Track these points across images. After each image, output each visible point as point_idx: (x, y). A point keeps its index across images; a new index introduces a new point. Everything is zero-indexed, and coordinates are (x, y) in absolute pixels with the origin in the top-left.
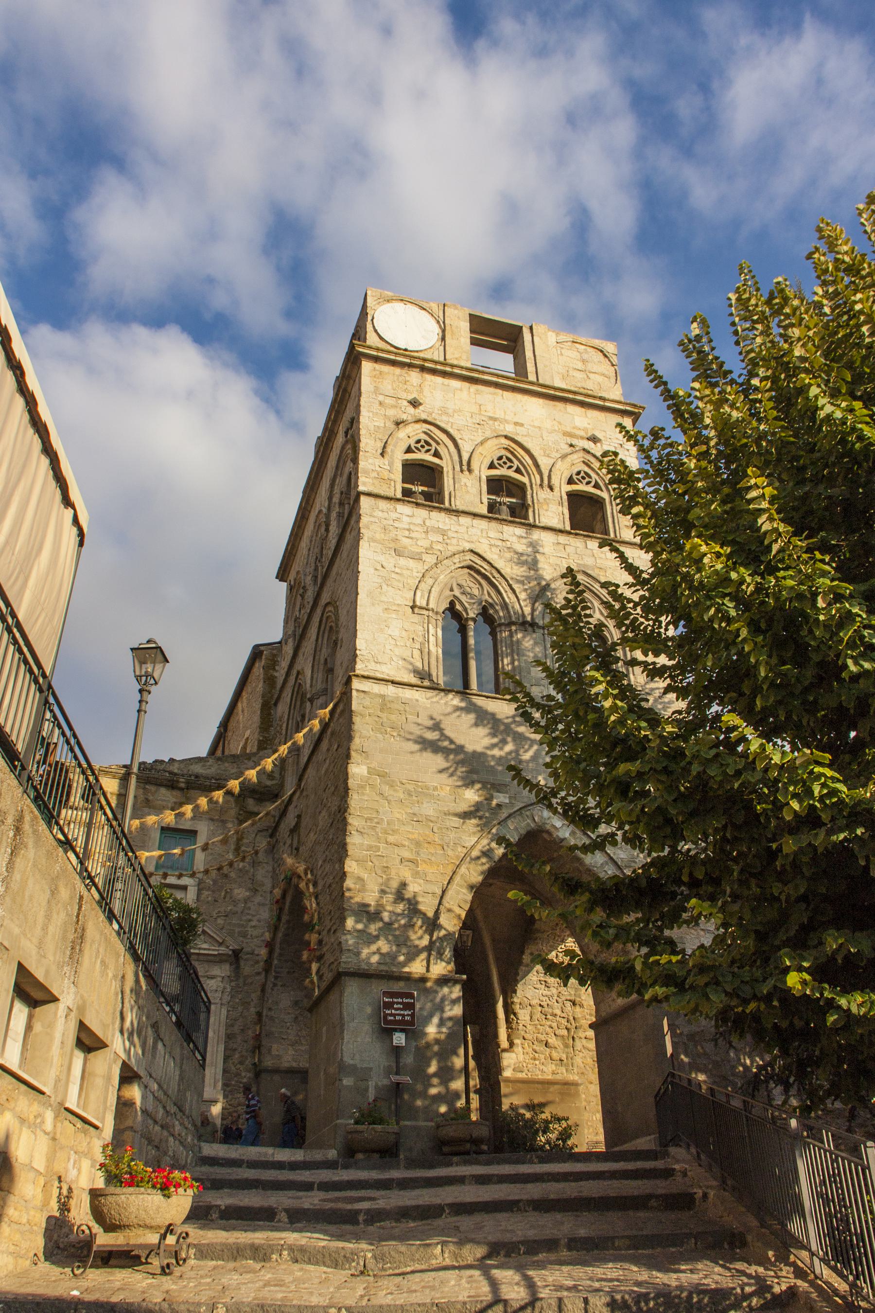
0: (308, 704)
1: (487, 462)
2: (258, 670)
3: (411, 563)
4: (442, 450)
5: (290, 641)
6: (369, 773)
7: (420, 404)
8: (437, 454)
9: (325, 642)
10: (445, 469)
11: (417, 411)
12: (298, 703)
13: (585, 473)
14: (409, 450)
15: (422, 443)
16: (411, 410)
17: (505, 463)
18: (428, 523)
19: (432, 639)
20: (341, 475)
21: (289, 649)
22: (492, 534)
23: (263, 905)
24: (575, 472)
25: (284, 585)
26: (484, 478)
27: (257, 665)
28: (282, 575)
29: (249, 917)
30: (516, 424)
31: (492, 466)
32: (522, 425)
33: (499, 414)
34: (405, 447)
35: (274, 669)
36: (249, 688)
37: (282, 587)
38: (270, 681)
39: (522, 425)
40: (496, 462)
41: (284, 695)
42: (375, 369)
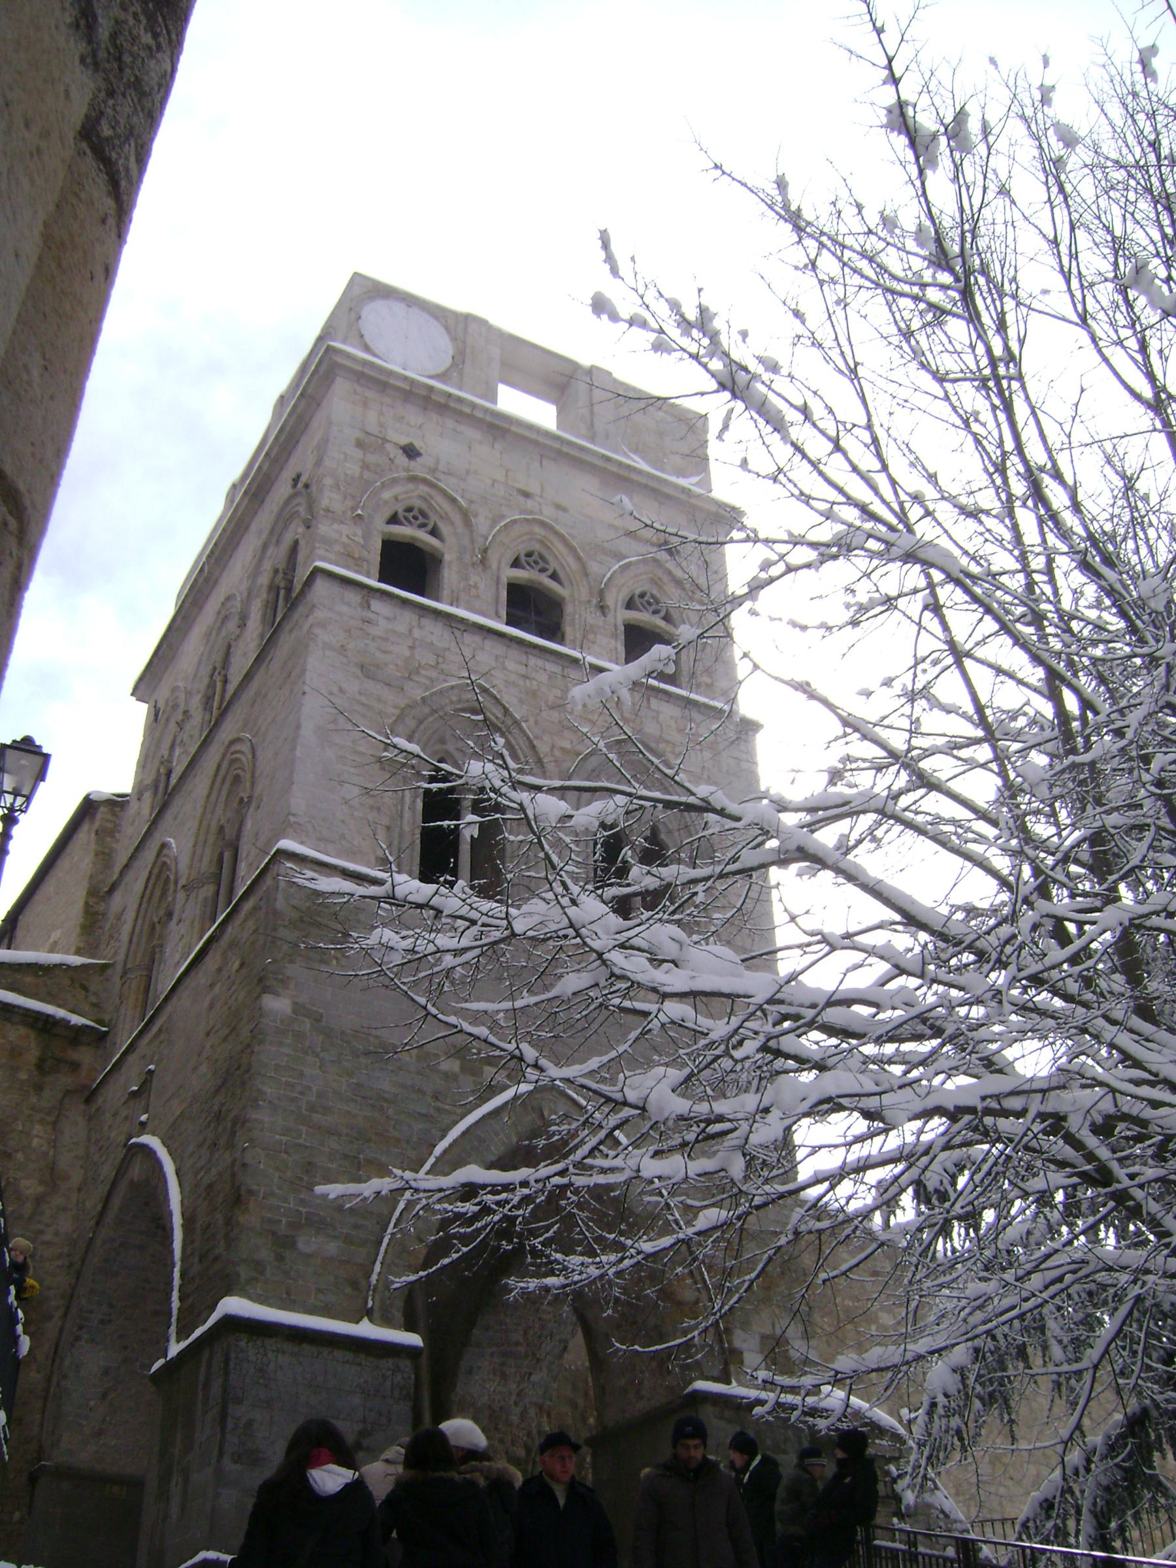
0: (181, 895)
1: (510, 557)
2: (85, 834)
3: (388, 695)
4: (444, 528)
5: (148, 796)
6: (294, 1012)
7: (419, 454)
8: (434, 532)
9: (223, 798)
10: (447, 557)
11: (413, 463)
12: (158, 893)
13: (653, 596)
14: (394, 520)
15: (416, 512)
16: (402, 460)
17: (536, 562)
18: (417, 634)
19: (407, 814)
20: (278, 542)
21: (145, 809)
22: (511, 665)
23: (65, 1209)
24: (637, 592)
25: (142, 709)
26: (505, 581)
27: (85, 827)
28: (144, 687)
29: (41, 1227)
30: (558, 507)
31: (516, 564)
32: (565, 510)
33: (533, 488)
34: (388, 514)
35: (113, 837)
36: (64, 864)
37: (142, 710)
38: (104, 856)
39: (565, 510)
40: (523, 559)
41: (129, 877)
42: (355, 392)
